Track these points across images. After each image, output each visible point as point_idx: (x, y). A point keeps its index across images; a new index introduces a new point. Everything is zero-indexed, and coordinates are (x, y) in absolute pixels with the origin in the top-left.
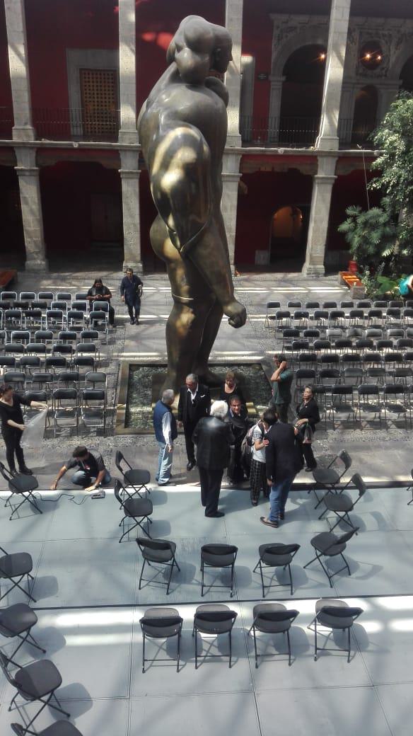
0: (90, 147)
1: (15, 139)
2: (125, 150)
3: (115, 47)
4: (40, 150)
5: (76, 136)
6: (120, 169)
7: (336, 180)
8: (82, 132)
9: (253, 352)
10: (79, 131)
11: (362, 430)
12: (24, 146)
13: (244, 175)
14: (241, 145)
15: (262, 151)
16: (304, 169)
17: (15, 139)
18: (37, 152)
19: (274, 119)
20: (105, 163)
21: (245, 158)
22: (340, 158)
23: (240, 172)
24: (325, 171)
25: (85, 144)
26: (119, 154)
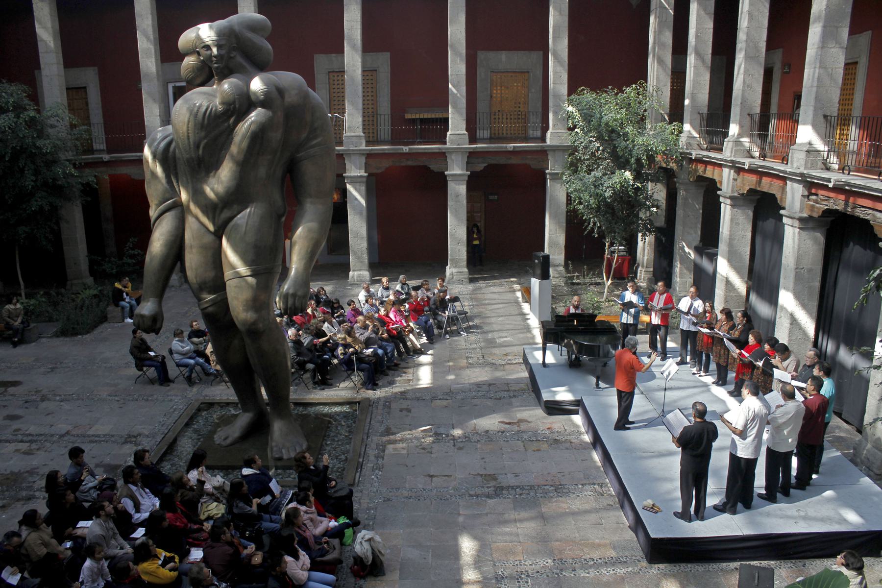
0: (430, 151)
1: (448, 145)
2: (554, 151)
3: (339, 50)
4: (369, 156)
5: (484, 139)
6: (447, 170)
7: (469, 176)
8: (489, 135)
9: (495, 311)
10: (103, 146)
11: (879, 400)
12: (555, 149)
13: (370, 175)
14: (467, 140)
15: (439, 149)
16: (534, 164)
17: (448, 145)
18: (366, 158)
19: (485, 115)
20: (434, 167)
21: (472, 156)
22: (470, 153)
23: (365, 173)
24: (456, 169)
25: (520, 147)
26: (547, 155)
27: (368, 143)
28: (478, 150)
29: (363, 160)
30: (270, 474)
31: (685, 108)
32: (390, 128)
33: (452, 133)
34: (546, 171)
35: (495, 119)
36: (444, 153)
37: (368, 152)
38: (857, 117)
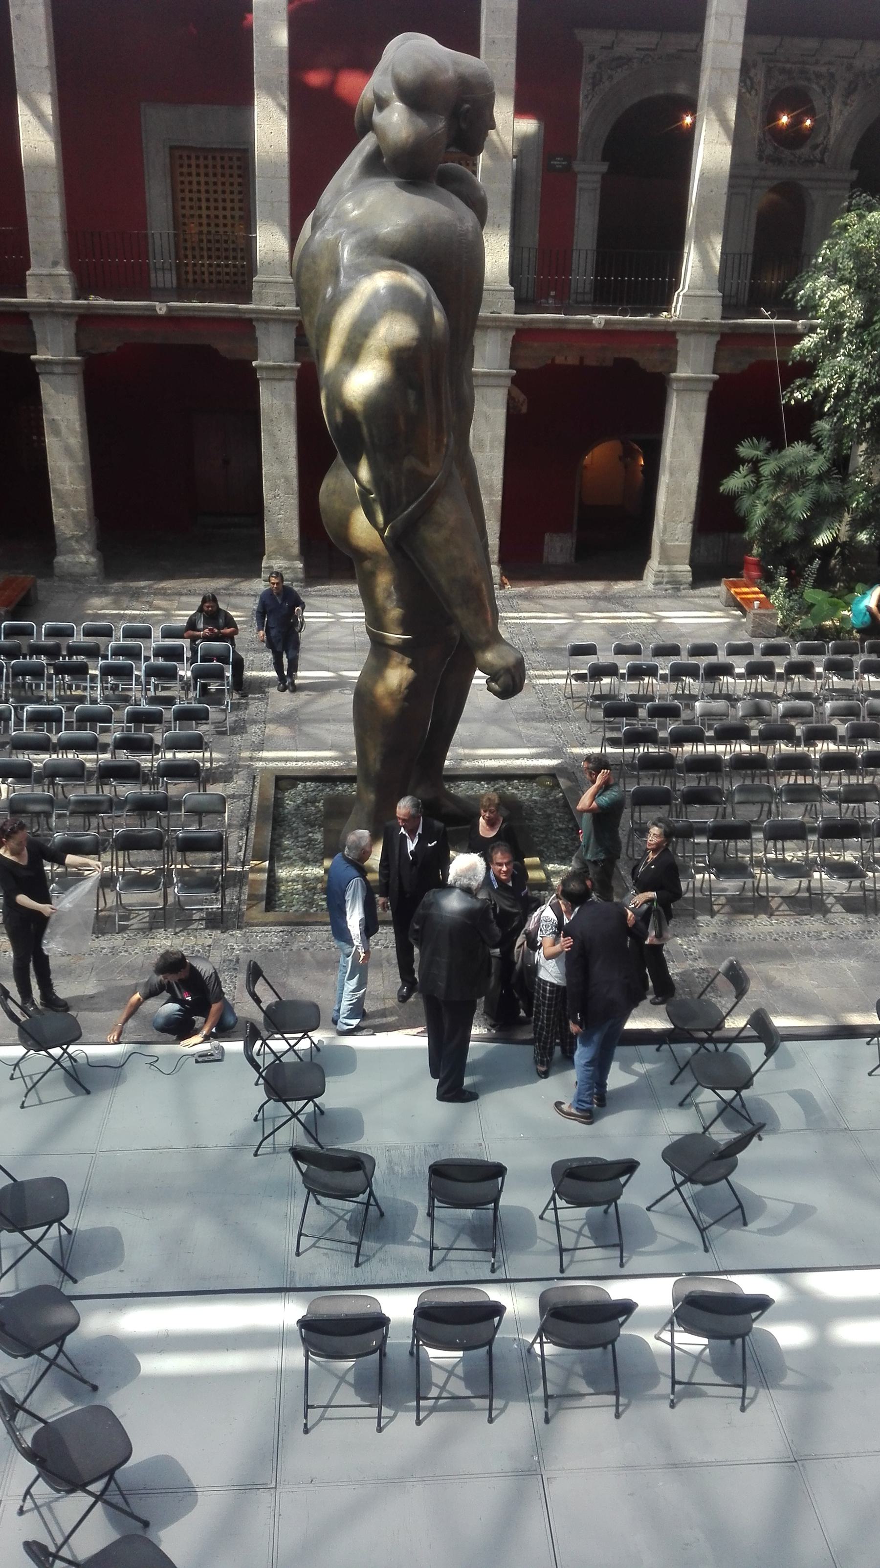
1: (33, 297)
2: (266, 321)
7: (716, 383)
8: (174, 282)
12: (51, 310)
16: (648, 361)
17: (33, 297)
18: (79, 325)
20: (224, 347)
22: (518, 331)
23: (714, 373)
25: (182, 308)
27: (81, 291)
28: (542, 326)
29: (70, 329)
30: (357, 674)
31: (721, 223)
32: (747, 282)
33: (690, 293)
34: (254, 363)
35: (186, 249)
36: (250, 320)
37: (81, 311)
38: (734, 255)
